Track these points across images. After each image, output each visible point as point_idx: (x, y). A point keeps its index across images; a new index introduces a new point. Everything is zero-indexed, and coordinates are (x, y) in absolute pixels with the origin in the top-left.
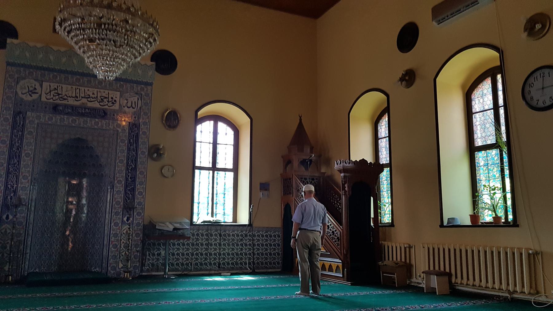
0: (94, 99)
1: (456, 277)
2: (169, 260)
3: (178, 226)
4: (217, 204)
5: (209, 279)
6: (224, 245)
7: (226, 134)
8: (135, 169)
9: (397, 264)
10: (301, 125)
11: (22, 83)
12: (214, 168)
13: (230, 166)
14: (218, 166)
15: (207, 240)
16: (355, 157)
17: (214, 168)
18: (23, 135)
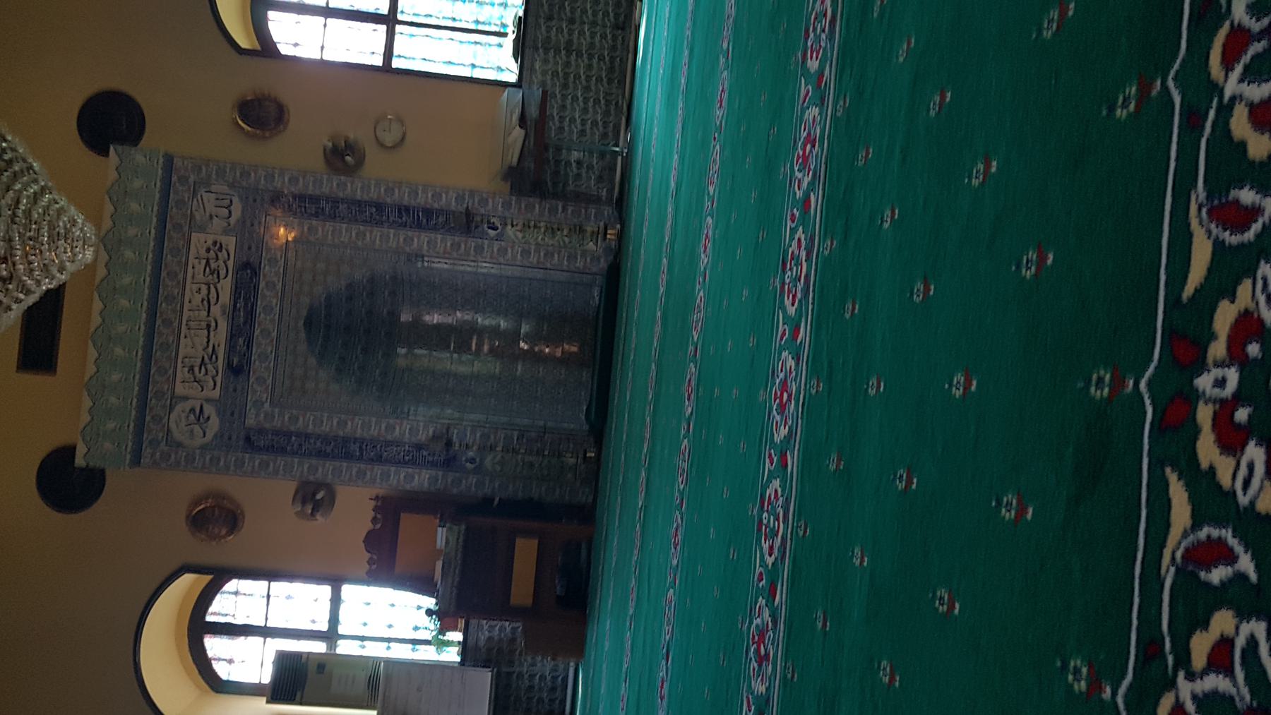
0: (213, 290)
4: (477, 22)
8: (379, 207)
11: (177, 435)
17: (390, 20)
18: (298, 435)
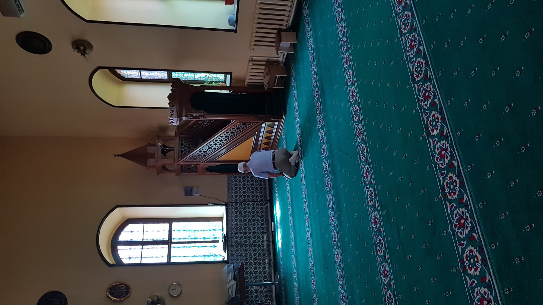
1: (281, 25)
2: (261, 281)
3: (231, 276)
4: (204, 238)
5: (279, 244)
6: (245, 229)
7: (132, 232)
9: (267, 74)
10: (123, 156)
12: (169, 243)
13: (167, 226)
14: (167, 238)
15: (241, 246)
16: (165, 103)
17: (169, 243)
